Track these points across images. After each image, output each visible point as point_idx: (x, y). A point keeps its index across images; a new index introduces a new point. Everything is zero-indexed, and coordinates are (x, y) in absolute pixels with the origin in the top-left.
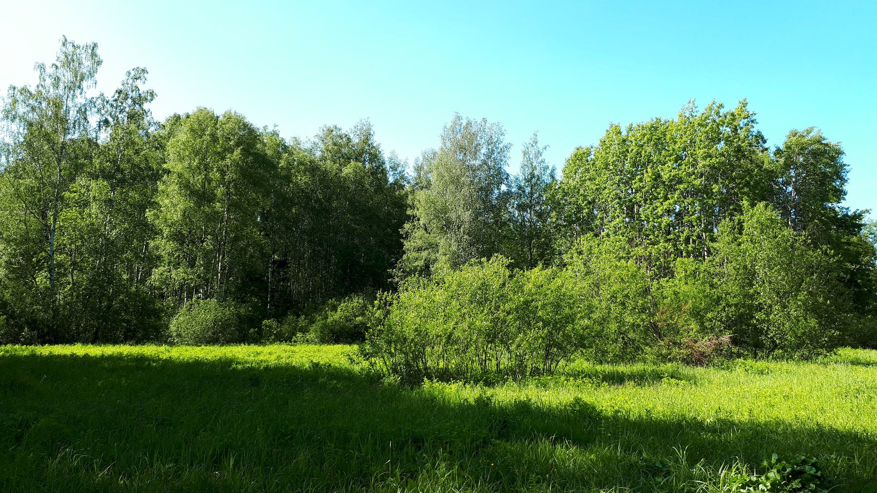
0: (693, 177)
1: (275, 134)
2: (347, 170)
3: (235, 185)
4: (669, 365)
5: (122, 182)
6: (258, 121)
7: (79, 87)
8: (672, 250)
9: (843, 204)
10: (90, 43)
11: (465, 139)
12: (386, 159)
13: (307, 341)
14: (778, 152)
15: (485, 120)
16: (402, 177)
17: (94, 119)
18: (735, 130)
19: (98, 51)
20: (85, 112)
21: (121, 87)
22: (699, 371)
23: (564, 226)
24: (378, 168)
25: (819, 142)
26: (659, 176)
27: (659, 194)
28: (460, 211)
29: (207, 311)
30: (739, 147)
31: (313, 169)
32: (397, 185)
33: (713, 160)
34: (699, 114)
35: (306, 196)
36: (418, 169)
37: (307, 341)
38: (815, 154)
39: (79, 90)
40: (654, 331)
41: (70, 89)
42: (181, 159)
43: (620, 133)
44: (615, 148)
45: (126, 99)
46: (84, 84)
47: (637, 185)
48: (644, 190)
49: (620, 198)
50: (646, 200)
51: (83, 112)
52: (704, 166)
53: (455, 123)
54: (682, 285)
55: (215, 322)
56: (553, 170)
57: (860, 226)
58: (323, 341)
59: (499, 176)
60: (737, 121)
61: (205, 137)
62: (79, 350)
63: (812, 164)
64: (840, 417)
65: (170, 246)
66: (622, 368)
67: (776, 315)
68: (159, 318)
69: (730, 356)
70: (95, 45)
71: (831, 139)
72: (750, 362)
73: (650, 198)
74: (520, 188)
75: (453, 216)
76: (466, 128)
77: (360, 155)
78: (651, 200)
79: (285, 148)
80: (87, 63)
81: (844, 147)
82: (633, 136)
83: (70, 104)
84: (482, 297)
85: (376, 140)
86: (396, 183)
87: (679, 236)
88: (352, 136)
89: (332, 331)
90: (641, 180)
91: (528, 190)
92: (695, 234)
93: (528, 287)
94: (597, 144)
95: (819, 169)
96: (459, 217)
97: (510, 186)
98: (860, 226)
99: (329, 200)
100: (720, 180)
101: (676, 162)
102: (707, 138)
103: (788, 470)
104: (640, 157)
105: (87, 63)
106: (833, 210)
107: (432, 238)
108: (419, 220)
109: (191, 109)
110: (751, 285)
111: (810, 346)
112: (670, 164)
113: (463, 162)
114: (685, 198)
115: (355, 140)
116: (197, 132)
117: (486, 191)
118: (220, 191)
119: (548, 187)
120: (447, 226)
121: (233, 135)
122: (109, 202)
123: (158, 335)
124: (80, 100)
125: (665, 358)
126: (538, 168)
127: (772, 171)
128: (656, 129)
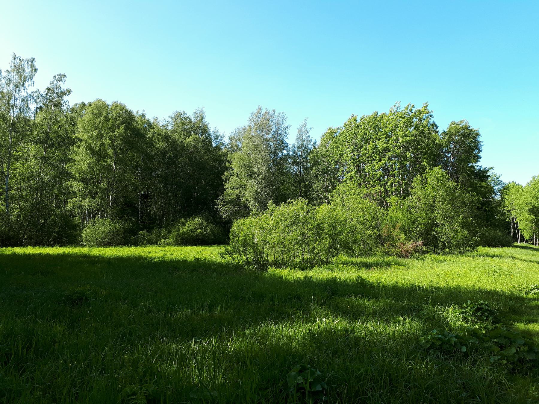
0: (396, 148)
1: (143, 115)
2: (189, 140)
3: (121, 149)
4: (390, 257)
5: (52, 146)
6: (134, 108)
9: (479, 164)
10: (30, 57)
12: (212, 132)
13: (167, 244)
14: (444, 133)
15: (274, 111)
16: (222, 144)
17: (33, 106)
19: (35, 63)
20: (27, 101)
21: (49, 86)
22: (407, 261)
25: (467, 128)
26: (376, 147)
27: (376, 157)
28: (259, 166)
29: (104, 226)
31: (166, 138)
32: (218, 148)
35: (162, 154)
36: (231, 139)
37: (167, 244)
38: (465, 135)
39: (23, 88)
40: (381, 240)
41: (17, 87)
42: (86, 131)
43: (356, 121)
46: (26, 84)
48: (367, 155)
49: (354, 159)
50: (368, 161)
51: (25, 101)
52: (403, 141)
55: (110, 232)
57: (488, 177)
58: (177, 244)
59: (282, 145)
62: (30, 250)
65: (80, 185)
67: (446, 229)
70: (33, 60)
71: (474, 127)
72: (433, 255)
74: (295, 152)
75: (255, 169)
78: (371, 161)
80: (28, 71)
81: (481, 132)
83: (17, 96)
84: (294, 222)
85: (206, 120)
89: (183, 238)
92: (396, 181)
93: (319, 216)
95: (467, 143)
96: (259, 170)
98: (488, 177)
99: (176, 157)
101: (386, 138)
103: (475, 308)
104: (366, 134)
105: (28, 71)
107: (243, 181)
109: (92, 100)
111: (464, 246)
112: (383, 140)
114: (391, 160)
115: (194, 120)
116: (96, 115)
118: (111, 151)
120: (251, 175)
122: (44, 158)
123: (74, 241)
124: (23, 94)
125: (387, 254)
126: (306, 140)
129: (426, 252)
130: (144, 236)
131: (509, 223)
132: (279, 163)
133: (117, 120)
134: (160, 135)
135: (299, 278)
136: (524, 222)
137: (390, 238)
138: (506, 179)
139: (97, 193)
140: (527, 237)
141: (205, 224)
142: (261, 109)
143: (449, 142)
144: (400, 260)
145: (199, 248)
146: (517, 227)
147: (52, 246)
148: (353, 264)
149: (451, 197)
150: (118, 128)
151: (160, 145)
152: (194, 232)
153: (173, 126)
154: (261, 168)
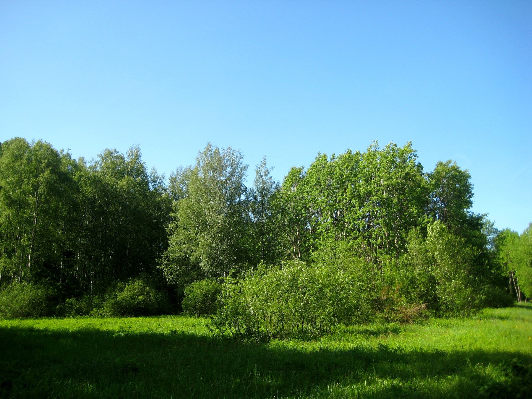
1: (68, 156)
2: (122, 183)
6: (57, 147)
9: (471, 210)
11: (215, 161)
12: (148, 174)
13: (101, 314)
14: (430, 176)
15: (230, 148)
16: (160, 187)
31: (96, 182)
34: (380, 150)
35: (90, 202)
36: (173, 180)
40: (378, 304)
59: (239, 188)
66: (363, 328)
76: (215, 153)
81: (471, 173)
85: (143, 159)
95: (456, 187)
98: (481, 225)
99: (108, 204)
104: (343, 177)
107: (192, 234)
111: (470, 307)
115: (127, 159)
116: (16, 158)
117: (231, 198)
120: (204, 226)
125: (387, 320)
127: (427, 189)
129: (426, 317)
130: (71, 304)
131: (506, 279)
132: (235, 211)
133: (40, 162)
134: (89, 179)
135: (314, 349)
136: (522, 276)
137: (390, 301)
138: (500, 226)
139: (14, 251)
140: (527, 295)
141: (147, 288)
142: (210, 146)
143: (437, 186)
144: (403, 326)
145: (148, 319)
146: (516, 283)
147: (496, 307)
148: (360, 332)
149: (451, 251)
150: (43, 171)
151: (87, 190)
152: (134, 299)
153: (102, 168)
154: (216, 218)
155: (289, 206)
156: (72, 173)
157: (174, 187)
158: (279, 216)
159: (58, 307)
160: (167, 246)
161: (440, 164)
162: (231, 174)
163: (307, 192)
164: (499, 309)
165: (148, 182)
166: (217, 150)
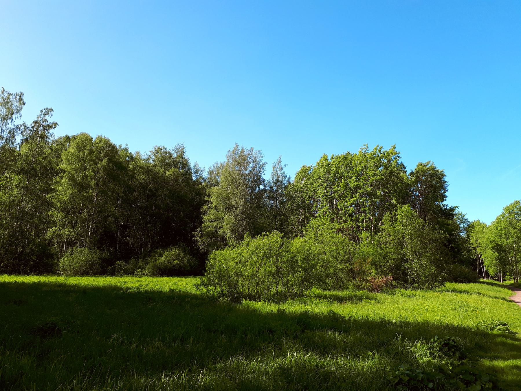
1: (126, 150)
2: (169, 173)
5: (36, 176)
6: (117, 141)
7: (10, 118)
8: (355, 226)
9: (445, 203)
14: (412, 173)
15: (252, 149)
16: (201, 177)
17: (19, 138)
18: (389, 161)
19: (24, 98)
21: (36, 119)
22: (378, 295)
23: (295, 210)
24: (187, 172)
25: (433, 169)
27: (348, 194)
29: (82, 255)
30: (392, 170)
31: (148, 171)
32: (198, 182)
33: (378, 178)
34: (370, 152)
35: (143, 187)
36: (211, 173)
37: (144, 274)
38: (432, 176)
39: (10, 120)
40: (352, 274)
42: (70, 163)
43: (327, 159)
44: (324, 168)
45: (39, 126)
46: (14, 116)
47: (336, 188)
48: (339, 192)
51: (12, 133)
52: (373, 180)
53: (235, 149)
54: (366, 246)
55: (88, 261)
56: (290, 178)
57: (453, 215)
58: (153, 275)
59: (259, 180)
60: (391, 156)
61: (85, 151)
63: (429, 181)
64: (454, 319)
65: (61, 215)
66: (337, 293)
68: (53, 258)
69: (394, 287)
70: (22, 94)
71: (439, 168)
73: (343, 196)
74: (271, 187)
77: (177, 164)
79: (132, 158)
80: (16, 104)
81: (446, 173)
82: (334, 162)
85: (187, 155)
86: (197, 180)
87: (359, 218)
88: (173, 152)
89: (159, 269)
90: (338, 186)
91: (275, 189)
92: (367, 217)
94: (314, 165)
95: (433, 183)
97: (265, 187)
98: (453, 215)
99: (157, 190)
100: (381, 189)
102: (374, 165)
103: (442, 343)
104: (339, 172)
106: (440, 206)
107: (221, 214)
108: (212, 203)
110: (402, 248)
112: (354, 178)
113: (239, 171)
115: (175, 155)
116: (80, 148)
118: (93, 182)
119: (287, 187)
120: (229, 208)
121: (103, 150)
122: (26, 188)
123: (50, 270)
124: (10, 126)
125: (359, 288)
126: (281, 177)
127: (408, 184)
128: (346, 158)
130: (121, 265)
135: (272, 311)
138: (471, 218)
140: (491, 273)
141: (182, 255)
142: (237, 146)
143: (416, 182)
146: (483, 263)
150: (102, 160)
155: (298, 195)
156: (128, 162)
157: (211, 178)
158: (289, 203)
159: (109, 267)
160: (201, 223)
161: (421, 164)
162: (254, 169)
163: (310, 184)
164: (464, 284)
165: (191, 173)
166: (243, 150)
